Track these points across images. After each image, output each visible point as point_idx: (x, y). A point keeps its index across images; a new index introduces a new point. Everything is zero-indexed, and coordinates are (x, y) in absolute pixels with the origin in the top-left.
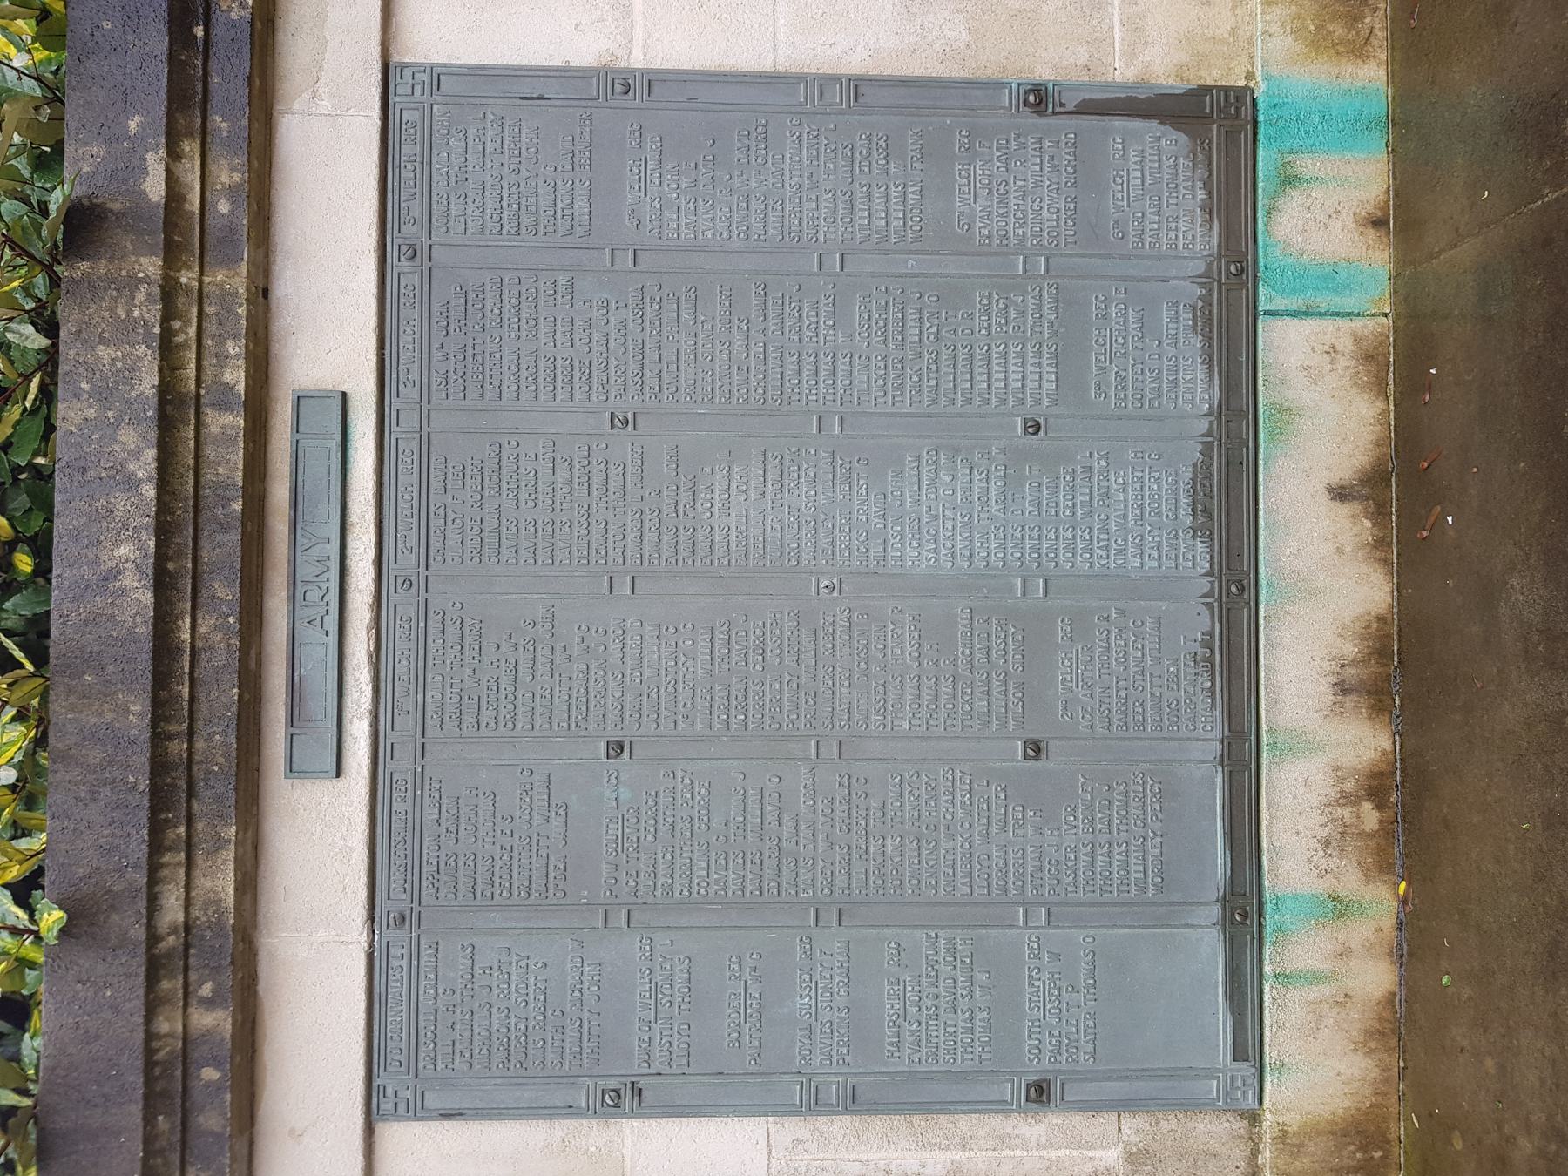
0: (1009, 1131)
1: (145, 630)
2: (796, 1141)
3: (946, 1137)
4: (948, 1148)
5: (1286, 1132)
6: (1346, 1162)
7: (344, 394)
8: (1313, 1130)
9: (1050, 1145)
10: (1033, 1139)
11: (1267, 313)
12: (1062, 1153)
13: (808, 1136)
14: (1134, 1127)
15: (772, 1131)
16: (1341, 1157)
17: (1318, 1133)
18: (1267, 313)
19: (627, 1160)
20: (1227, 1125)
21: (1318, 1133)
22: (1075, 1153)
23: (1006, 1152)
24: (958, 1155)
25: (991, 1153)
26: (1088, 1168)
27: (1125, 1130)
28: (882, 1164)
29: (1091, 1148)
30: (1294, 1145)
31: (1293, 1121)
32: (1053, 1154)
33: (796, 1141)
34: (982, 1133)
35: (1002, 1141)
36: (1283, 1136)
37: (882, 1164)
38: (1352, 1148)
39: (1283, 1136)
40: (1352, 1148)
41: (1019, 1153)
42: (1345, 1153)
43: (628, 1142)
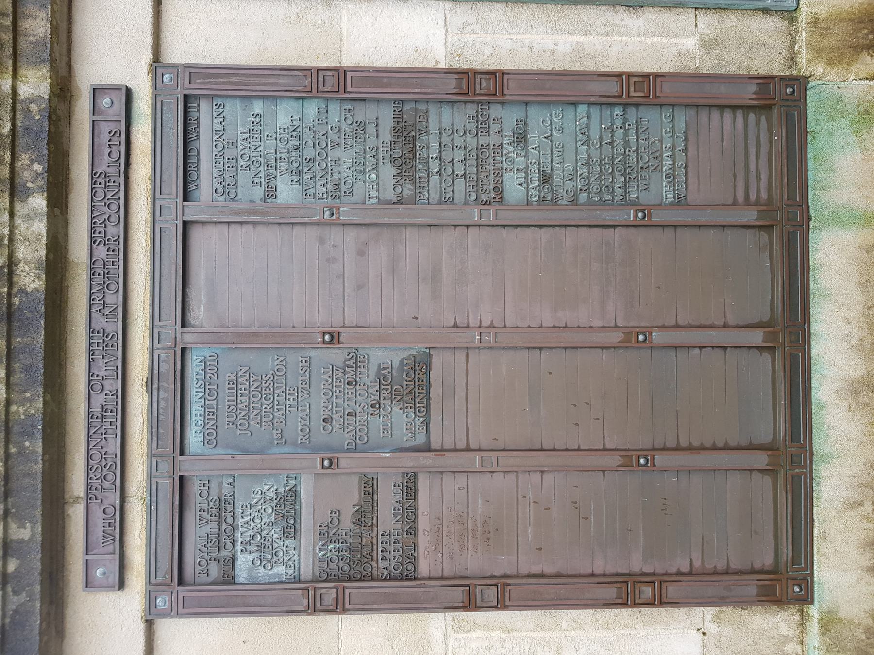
0: (618, 22)
1: (10, 91)
2: (466, 24)
3: (572, 24)
4: (573, 33)
5: (818, 19)
6: (861, 41)
7: (129, 92)
8: (837, 18)
9: (648, 33)
10: (635, 29)
11: (467, 353)
12: (655, 39)
13: (473, 20)
14: (707, 22)
15: (448, 16)
16: (857, 38)
17: (841, 21)
18: (467, 353)
19: (345, 33)
20: (773, 24)
21: (841, 21)
22: (665, 40)
23: (616, 38)
24: (582, 39)
25: (604, 38)
26: (674, 50)
27: (700, 25)
28: (527, 42)
29: (676, 36)
30: (822, 28)
31: (823, 11)
32: (649, 41)
33: (466, 24)
34: (598, 23)
35: (612, 30)
36: (814, 22)
37: (527, 42)
38: (866, 31)
39: (814, 22)
40: (866, 31)
41: (624, 38)
42: (860, 35)
43: (345, 19)
